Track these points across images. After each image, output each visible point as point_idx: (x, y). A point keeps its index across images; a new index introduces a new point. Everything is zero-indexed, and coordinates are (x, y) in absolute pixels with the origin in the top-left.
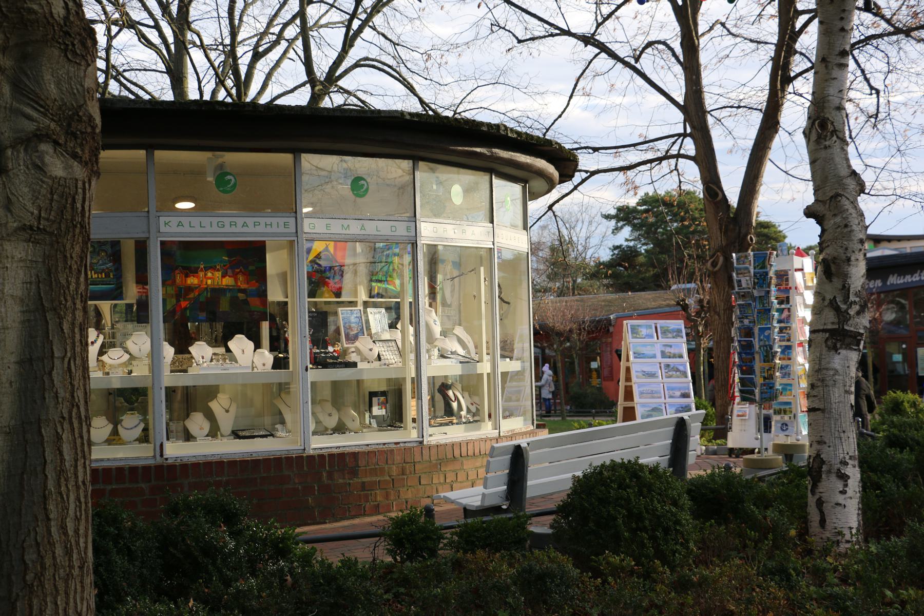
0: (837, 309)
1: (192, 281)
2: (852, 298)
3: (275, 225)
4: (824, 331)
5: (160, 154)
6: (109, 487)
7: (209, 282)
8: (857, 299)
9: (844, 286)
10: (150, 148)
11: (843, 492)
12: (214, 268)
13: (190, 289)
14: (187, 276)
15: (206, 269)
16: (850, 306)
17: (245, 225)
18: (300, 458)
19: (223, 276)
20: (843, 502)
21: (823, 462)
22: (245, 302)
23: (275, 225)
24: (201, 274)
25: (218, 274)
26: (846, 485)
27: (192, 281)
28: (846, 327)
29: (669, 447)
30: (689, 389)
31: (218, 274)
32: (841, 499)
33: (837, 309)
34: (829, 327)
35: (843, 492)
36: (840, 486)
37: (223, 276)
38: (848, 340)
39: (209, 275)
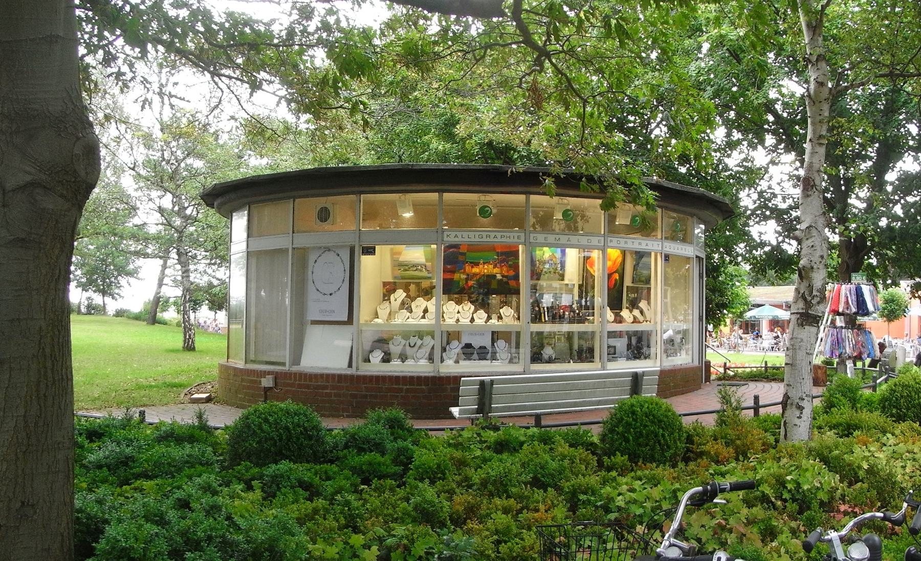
0: (805, 299)
1: (476, 270)
2: (815, 293)
3: (512, 237)
4: (797, 313)
5: (447, 196)
6: (405, 387)
7: (486, 271)
8: (818, 294)
9: (810, 285)
10: (528, 193)
11: (800, 417)
12: (488, 263)
13: (475, 275)
14: (472, 267)
15: (484, 263)
16: (813, 298)
17: (456, 236)
18: (434, 378)
19: (494, 268)
20: (798, 424)
21: (789, 398)
22: (507, 283)
23: (512, 237)
24: (481, 266)
25: (491, 266)
26: (801, 413)
27: (476, 270)
28: (810, 312)
29: (629, 384)
30: (285, 356)
31: (491, 266)
32: (797, 421)
33: (805, 299)
34: (801, 311)
35: (800, 417)
36: (798, 413)
37: (494, 268)
38: (811, 320)
39: (486, 267)
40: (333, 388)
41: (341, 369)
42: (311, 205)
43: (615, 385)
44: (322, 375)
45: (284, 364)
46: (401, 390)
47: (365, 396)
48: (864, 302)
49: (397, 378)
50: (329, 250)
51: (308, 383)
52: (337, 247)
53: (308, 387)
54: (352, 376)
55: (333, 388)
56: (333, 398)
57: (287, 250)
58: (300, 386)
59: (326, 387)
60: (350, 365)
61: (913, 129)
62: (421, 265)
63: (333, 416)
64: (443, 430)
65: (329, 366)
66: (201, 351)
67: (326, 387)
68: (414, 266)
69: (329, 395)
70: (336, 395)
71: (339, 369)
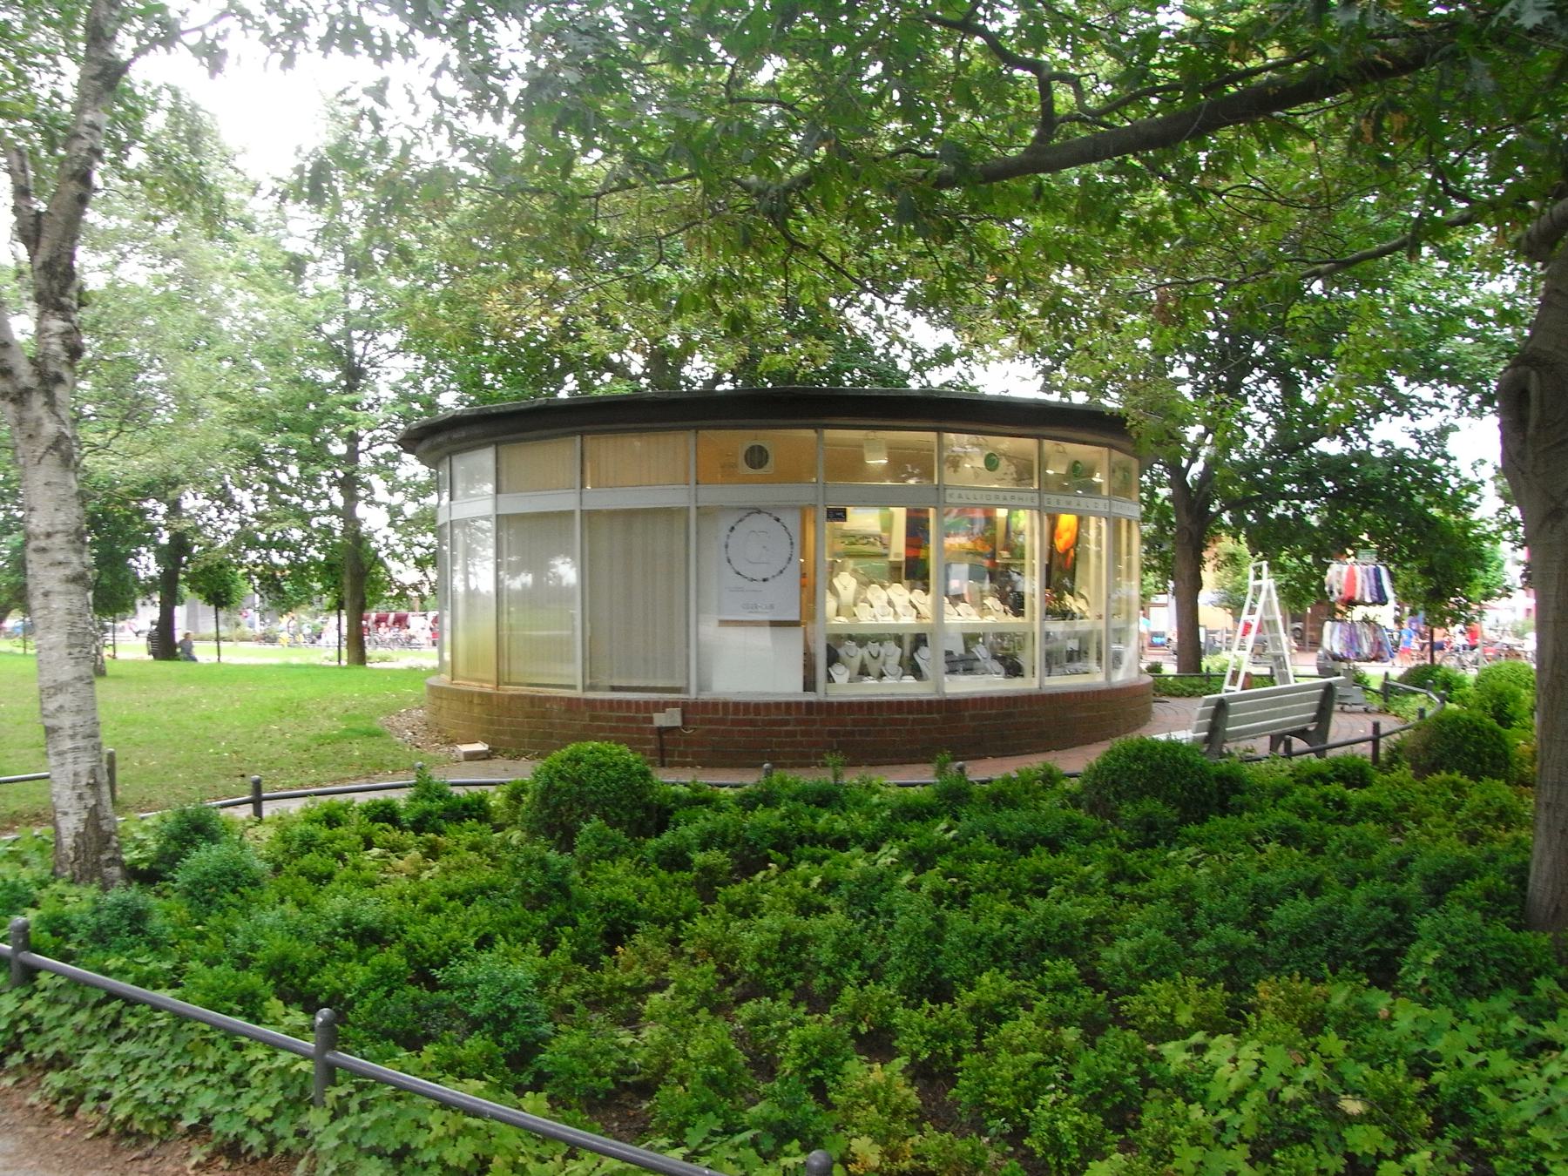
18: (939, 702)
40: (799, 722)
41: (796, 694)
42: (740, 440)
43: (1300, 700)
44: (778, 705)
45: (573, 687)
46: (904, 722)
47: (852, 733)
48: (1355, 585)
49: (900, 703)
50: (759, 512)
51: (751, 716)
52: (780, 508)
53: (751, 723)
54: (809, 705)
55: (799, 722)
56: (799, 738)
57: (688, 509)
58: (735, 723)
59: (786, 723)
60: (809, 684)
61: (574, 8)
62: (874, 536)
63: (801, 766)
64: (913, 785)
65: (770, 689)
66: (118, 677)
67: (786, 723)
68: (865, 537)
69: (792, 734)
70: (804, 733)
71: (789, 695)
